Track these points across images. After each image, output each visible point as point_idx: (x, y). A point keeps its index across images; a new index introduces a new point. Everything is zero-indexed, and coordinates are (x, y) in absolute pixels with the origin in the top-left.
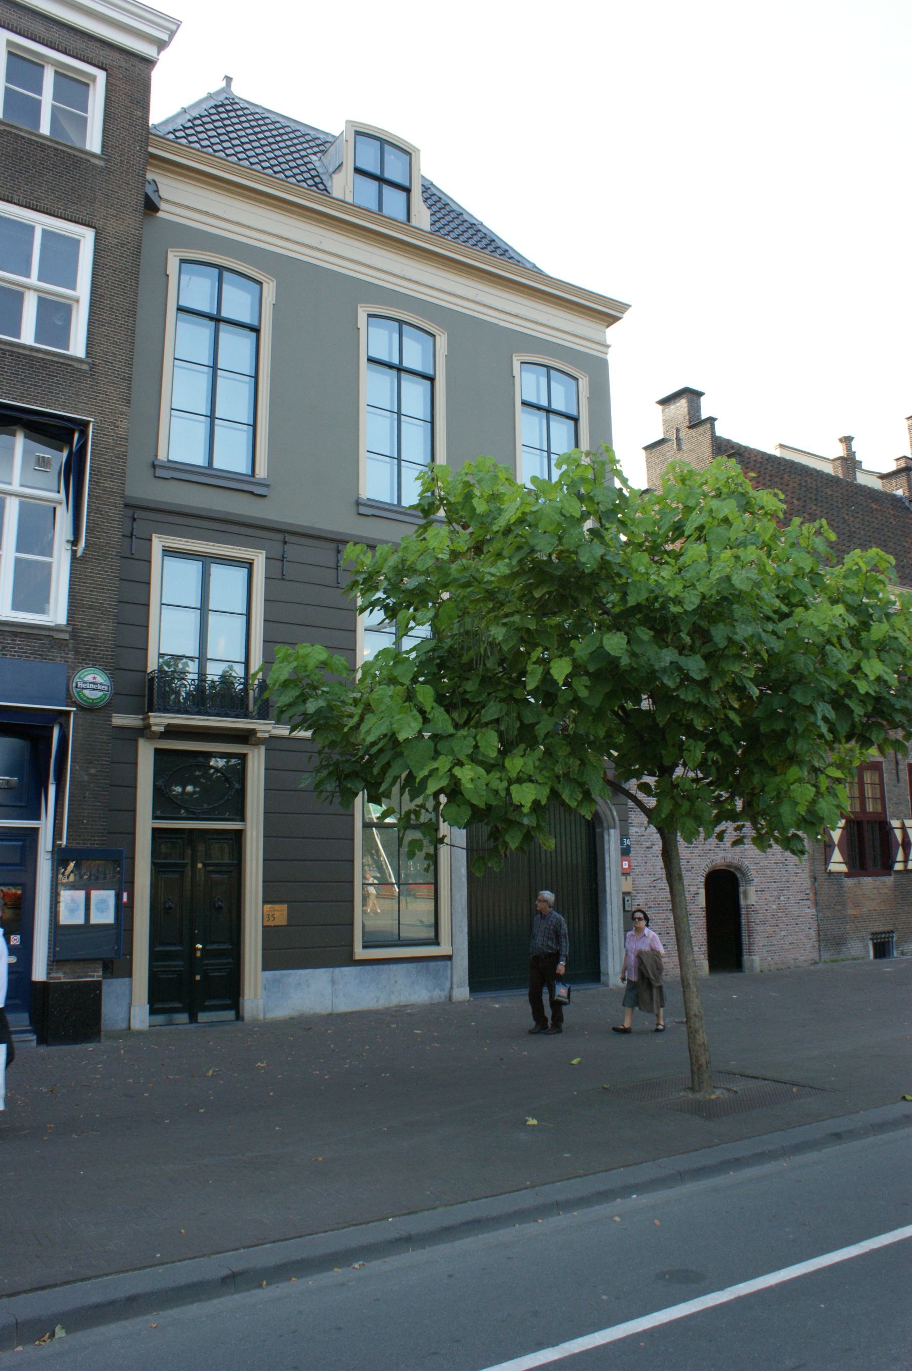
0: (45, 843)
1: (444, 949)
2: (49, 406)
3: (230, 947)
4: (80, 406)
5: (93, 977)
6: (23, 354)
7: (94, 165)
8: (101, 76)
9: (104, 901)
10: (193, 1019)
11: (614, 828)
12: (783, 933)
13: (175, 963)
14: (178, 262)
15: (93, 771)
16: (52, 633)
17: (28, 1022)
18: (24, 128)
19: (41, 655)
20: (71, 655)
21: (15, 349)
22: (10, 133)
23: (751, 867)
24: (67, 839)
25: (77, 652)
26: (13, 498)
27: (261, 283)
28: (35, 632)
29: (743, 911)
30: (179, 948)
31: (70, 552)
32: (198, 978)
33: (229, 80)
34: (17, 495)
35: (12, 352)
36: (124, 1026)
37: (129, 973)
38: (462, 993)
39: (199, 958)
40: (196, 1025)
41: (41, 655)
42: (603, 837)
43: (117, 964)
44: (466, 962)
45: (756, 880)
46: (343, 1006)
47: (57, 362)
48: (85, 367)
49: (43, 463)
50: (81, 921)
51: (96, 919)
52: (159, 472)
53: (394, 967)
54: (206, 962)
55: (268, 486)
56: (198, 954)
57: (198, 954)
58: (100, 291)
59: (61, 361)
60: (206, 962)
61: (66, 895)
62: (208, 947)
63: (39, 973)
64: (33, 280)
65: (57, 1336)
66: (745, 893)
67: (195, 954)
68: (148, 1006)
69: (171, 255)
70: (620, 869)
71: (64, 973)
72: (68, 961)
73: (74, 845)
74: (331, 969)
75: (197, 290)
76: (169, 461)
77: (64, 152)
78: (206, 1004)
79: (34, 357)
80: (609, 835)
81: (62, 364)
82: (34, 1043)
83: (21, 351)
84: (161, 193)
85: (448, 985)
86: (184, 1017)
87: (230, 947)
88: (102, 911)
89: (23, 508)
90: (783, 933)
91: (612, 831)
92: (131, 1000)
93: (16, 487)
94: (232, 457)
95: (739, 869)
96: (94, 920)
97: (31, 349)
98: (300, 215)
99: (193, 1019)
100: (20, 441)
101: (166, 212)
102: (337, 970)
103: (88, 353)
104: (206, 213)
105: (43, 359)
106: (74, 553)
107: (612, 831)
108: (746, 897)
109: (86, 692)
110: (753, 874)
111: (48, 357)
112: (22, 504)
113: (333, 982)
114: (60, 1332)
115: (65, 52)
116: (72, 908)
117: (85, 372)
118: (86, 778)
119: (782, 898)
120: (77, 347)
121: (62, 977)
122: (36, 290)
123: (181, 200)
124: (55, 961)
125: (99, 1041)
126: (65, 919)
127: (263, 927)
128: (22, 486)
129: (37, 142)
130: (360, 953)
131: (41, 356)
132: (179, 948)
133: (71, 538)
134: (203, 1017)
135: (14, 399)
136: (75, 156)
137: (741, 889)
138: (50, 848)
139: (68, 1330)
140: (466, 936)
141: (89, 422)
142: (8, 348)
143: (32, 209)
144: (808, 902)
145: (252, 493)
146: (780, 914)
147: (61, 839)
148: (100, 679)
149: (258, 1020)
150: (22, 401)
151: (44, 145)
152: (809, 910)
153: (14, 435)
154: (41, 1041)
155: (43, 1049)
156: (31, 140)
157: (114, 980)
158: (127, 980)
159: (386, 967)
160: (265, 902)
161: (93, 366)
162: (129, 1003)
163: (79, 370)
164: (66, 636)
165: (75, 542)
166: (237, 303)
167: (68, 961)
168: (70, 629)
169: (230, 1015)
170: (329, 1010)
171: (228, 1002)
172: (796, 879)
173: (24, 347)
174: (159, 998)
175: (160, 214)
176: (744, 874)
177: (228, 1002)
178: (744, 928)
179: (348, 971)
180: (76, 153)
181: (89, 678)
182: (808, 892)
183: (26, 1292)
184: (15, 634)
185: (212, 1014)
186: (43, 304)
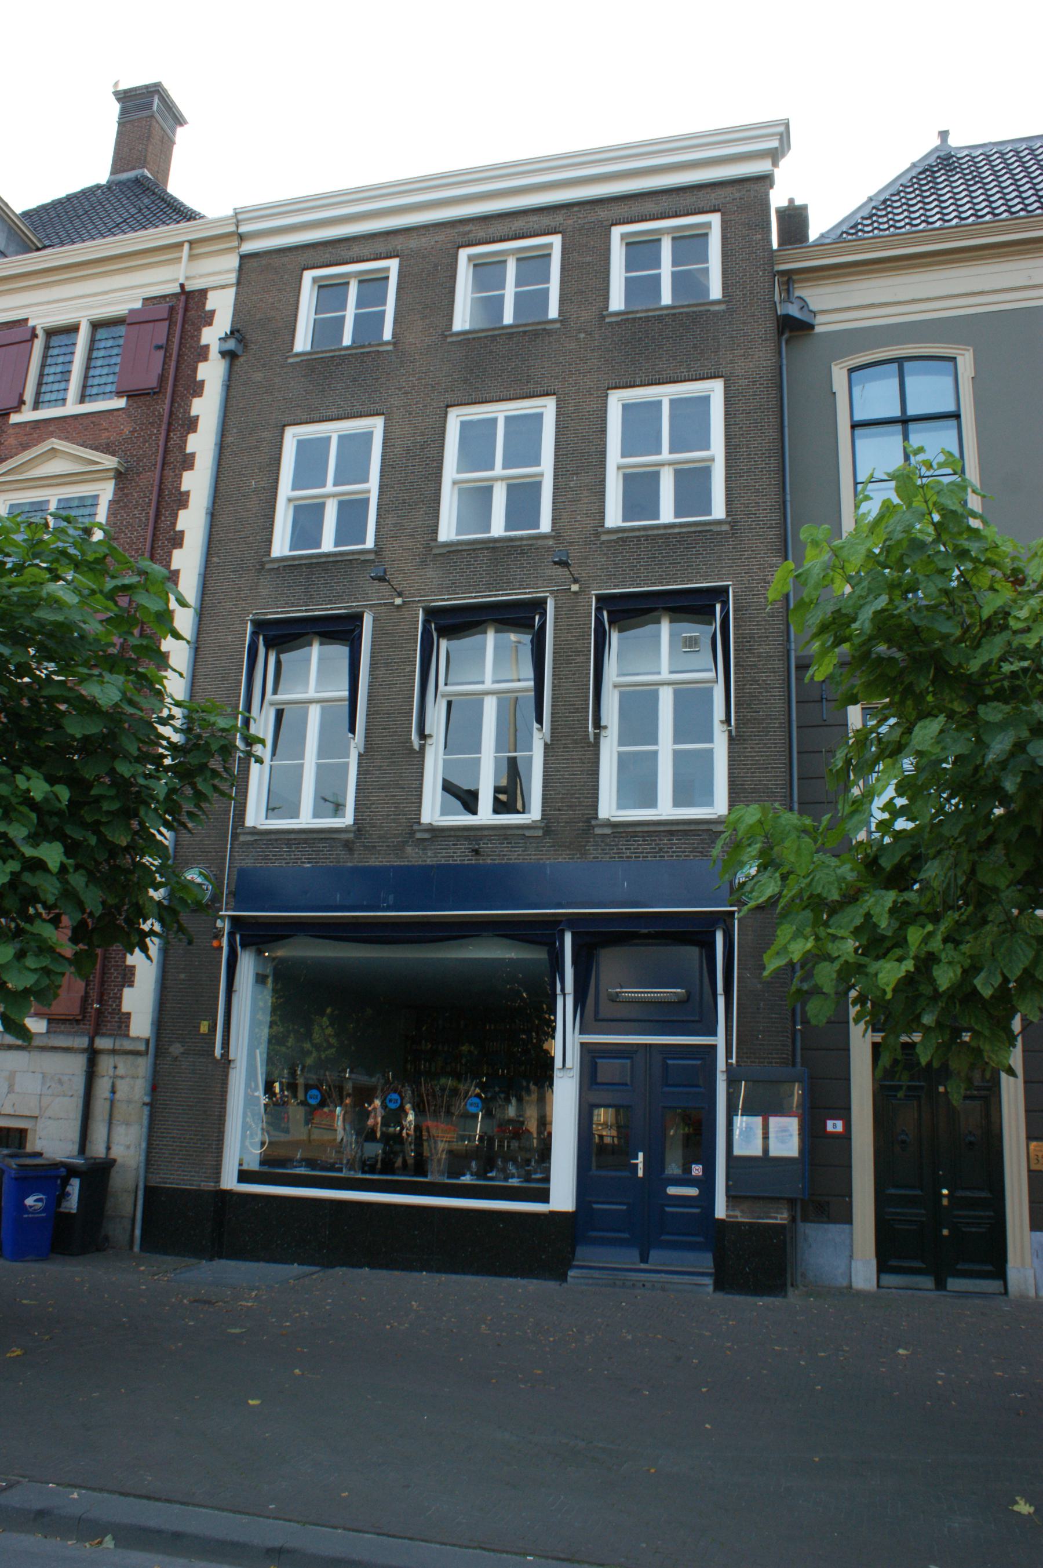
2: (690, 581)
3: (989, 1195)
4: (724, 571)
5: (776, 1218)
6: (658, 535)
9: (784, 1130)
10: (941, 1285)
13: (911, 1211)
14: (845, 372)
16: (711, 827)
17: (712, 1265)
18: (640, 308)
19: (701, 852)
21: (650, 533)
22: (627, 320)
24: (737, 1057)
26: (665, 687)
27: (955, 358)
28: (693, 827)
30: (918, 1192)
31: (726, 733)
32: (945, 1232)
33: (944, 135)
34: (669, 684)
35: (648, 536)
36: (845, 1283)
37: (848, 1219)
39: (946, 1207)
40: (944, 1293)
41: (701, 852)
43: (827, 1203)
47: (695, 532)
49: (692, 642)
51: (777, 1150)
54: (956, 1213)
56: (945, 1202)
57: (945, 1202)
59: (699, 529)
60: (956, 1213)
61: (740, 1121)
62: (960, 1193)
63: (721, 1211)
64: (665, 455)
65: (104, 1545)
67: (941, 1200)
68: (874, 1262)
69: (835, 369)
71: (742, 1211)
72: (746, 1198)
75: (878, 397)
77: (681, 313)
78: (959, 1267)
79: (670, 534)
81: (700, 532)
82: (711, 1289)
83: (656, 532)
84: (812, 307)
86: (928, 1282)
87: (989, 1195)
88: (783, 1142)
89: (678, 696)
92: (852, 1251)
93: (665, 675)
96: (773, 1152)
97: (672, 526)
98: (993, 256)
99: (941, 1285)
100: (665, 627)
101: (823, 325)
103: (728, 512)
104: (872, 306)
105: (679, 533)
111: (684, 530)
112: (676, 693)
114: (109, 1542)
118: (759, 986)
120: (719, 511)
122: (670, 464)
125: (785, 1296)
127: (1029, 1171)
128: (671, 672)
129: (654, 316)
131: (676, 530)
132: (918, 1192)
133: (723, 718)
134: (954, 1284)
135: (654, 584)
136: (694, 312)
139: (119, 1543)
141: (728, 586)
142: (642, 533)
143: (656, 384)
147: (732, 1058)
149: (1028, 1297)
150: (661, 584)
151: (661, 316)
153: (659, 622)
154: (719, 1286)
155: (720, 1296)
156: (648, 317)
157: (831, 1226)
158: (847, 1226)
160: (1030, 1138)
162: (851, 1254)
163: (719, 533)
166: (928, 392)
169: (992, 1286)
171: (990, 1268)
173: (666, 526)
174: (891, 1253)
175: (818, 329)
177: (990, 1268)
180: (695, 309)
183: (135, 1496)
184: (671, 833)
185: (978, 1282)
186: (680, 476)
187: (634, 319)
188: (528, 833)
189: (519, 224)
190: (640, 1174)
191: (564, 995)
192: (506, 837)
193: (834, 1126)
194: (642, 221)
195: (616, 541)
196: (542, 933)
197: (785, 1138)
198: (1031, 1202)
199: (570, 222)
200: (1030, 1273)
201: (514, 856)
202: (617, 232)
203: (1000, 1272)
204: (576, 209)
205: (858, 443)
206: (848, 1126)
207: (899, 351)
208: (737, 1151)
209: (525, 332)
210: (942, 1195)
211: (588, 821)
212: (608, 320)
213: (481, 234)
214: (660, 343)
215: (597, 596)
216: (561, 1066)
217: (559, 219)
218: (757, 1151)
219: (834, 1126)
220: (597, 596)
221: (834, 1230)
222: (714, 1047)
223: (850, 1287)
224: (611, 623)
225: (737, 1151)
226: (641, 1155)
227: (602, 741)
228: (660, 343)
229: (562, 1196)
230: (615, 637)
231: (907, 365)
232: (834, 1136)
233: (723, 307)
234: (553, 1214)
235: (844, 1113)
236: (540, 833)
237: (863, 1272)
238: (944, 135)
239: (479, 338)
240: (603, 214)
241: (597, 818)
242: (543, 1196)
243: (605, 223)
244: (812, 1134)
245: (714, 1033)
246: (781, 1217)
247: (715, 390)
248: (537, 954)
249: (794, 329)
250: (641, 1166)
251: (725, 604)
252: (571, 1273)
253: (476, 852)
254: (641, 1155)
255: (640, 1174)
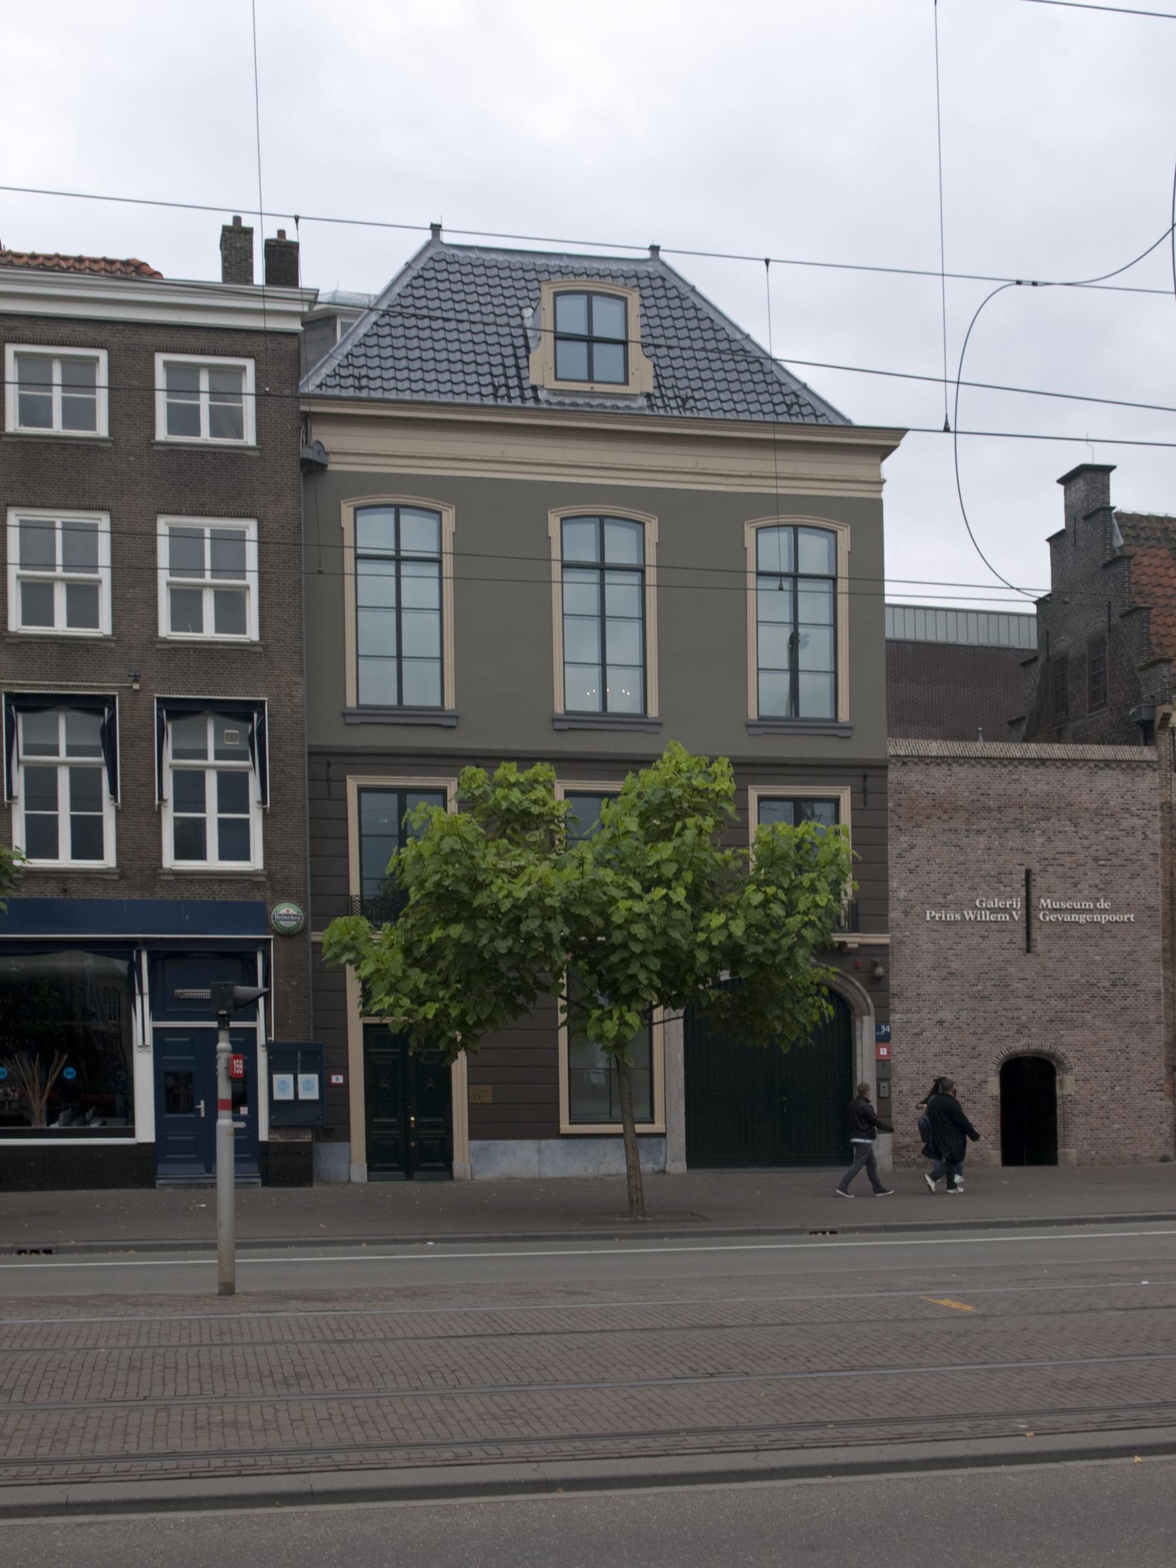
0: (261, 1039)
1: (658, 1127)
7: (250, 458)
8: (250, 364)
9: (308, 1082)
11: (869, 1014)
12: (1116, 1126)
14: (351, 510)
15: (294, 983)
20: (269, 893)
23: (1070, 1054)
25: (274, 891)
29: (1059, 1102)
32: (413, 1144)
33: (436, 228)
36: (346, 1179)
37: (348, 1139)
38: (678, 1166)
42: (858, 1024)
43: (336, 1130)
44: (682, 1140)
45: (1076, 1069)
46: (549, 1172)
48: (260, 649)
50: (291, 1097)
52: (349, 719)
53: (603, 1142)
55: (456, 717)
56: (413, 1125)
57: (413, 1125)
58: (267, 577)
63: (263, 1135)
66: (1061, 1082)
68: (365, 1165)
70: (874, 1057)
72: (284, 1127)
73: (282, 1040)
74: (537, 1141)
76: (359, 706)
80: (862, 1022)
85: (662, 1159)
90: (1116, 1126)
91: (866, 1018)
94: (423, 690)
95: (1053, 1056)
96: (302, 1097)
101: (335, 466)
102: (543, 1143)
103: (262, 636)
106: (264, 810)
107: (866, 1018)
108: (1062, 1087)
109: (282, 923)
110: (1071, 1059)
113: (540, 1152)
115: (215, 353)
116: (284, 1087)
117: (260, 653)
119: (1117, 1088)
121: (279, 1138)
123: (347, 449)
124: (273, 1127)
126: (277, 1096)
130: (565, 1127)
131: (220, 647)
133: (260, 799)
137: (1058, 1078)
138: (264, 1043)
140: (683, 1117)
144: (1162, 1094)
145: (440, 726)
146: (1113, 1106)
148: (292, 912)
152: (1163, 1103)
159: (594, 1141)
161: (266, 647)
162: (351, 1159)
164: (263, 879)
165: (264, 801)
167: (284, 1127)
168: (266, 873)
170: (536, 1175)
171: (442, 1165)
172: (1143, 1068)
176: (1061, 1062)
177: (442, 1165)
178: (1059, 1119)
179: (553, 1142)
181: (283, 911)
182: (1162, 1082)
184: (221, 881)
187: (179, 451)
188: (106, 877)
189: (65, 331)
190: (203, 1115)
191: (142, 995)
192: (88, 879)
193: (337, 1079)
194: (180, 352)
195: (169, 650)
196: (125, 949)
197: (309, 1087)
198: (470, 1123)
199: (115, 340)
200: (468, 1166)
201: (97, 893)
202: (160, 359)
203: (449, 1167)
204: (120, 327)
205: (358, 519)
206: (346, 1079)
207: (398, 495)
208: (276, 1097)
209: (78, 446)
210: (410, 1121)
211: (155, 869)
212: (155, 448)
213: (28, 333)
214: (203, 479)
215: (158, 699)
216: (140, 1043)
217: (104, 334)
218: (290, 1096)
219: (337, 1079)
220: (158, 699)
221: (338, 1147)
222: (254, 1030)
223: (350, 1181)
224: (168, 717)
225: (276, 1097)
226: (202, 1103)
227: (163, 809)
228: (203, 479)
229: (145, 1130)
230: (170, 727)
231: (402, 510)
232: (338, 1085)
233: (257, 454)
234: (141, 1145)
235: (344, 1070)
236: (116, 877)
237: (359, 1170)
238: (436, 228)
239: (34, 443)
240: (146, 338)
241: (161, 867)
242: (131, 1133)
243: (149, 349)
244: (324, 1084)
245: (254, 1019)
246: (307, 1138)
247: (251, 529)
248: (121, 966)
249: (313, 469)
250: (203, 1110)
251: (261, 714)
252: (159, 1182)
253: (65, 890)
254: (202, 1103)
255: (203, 1115)
